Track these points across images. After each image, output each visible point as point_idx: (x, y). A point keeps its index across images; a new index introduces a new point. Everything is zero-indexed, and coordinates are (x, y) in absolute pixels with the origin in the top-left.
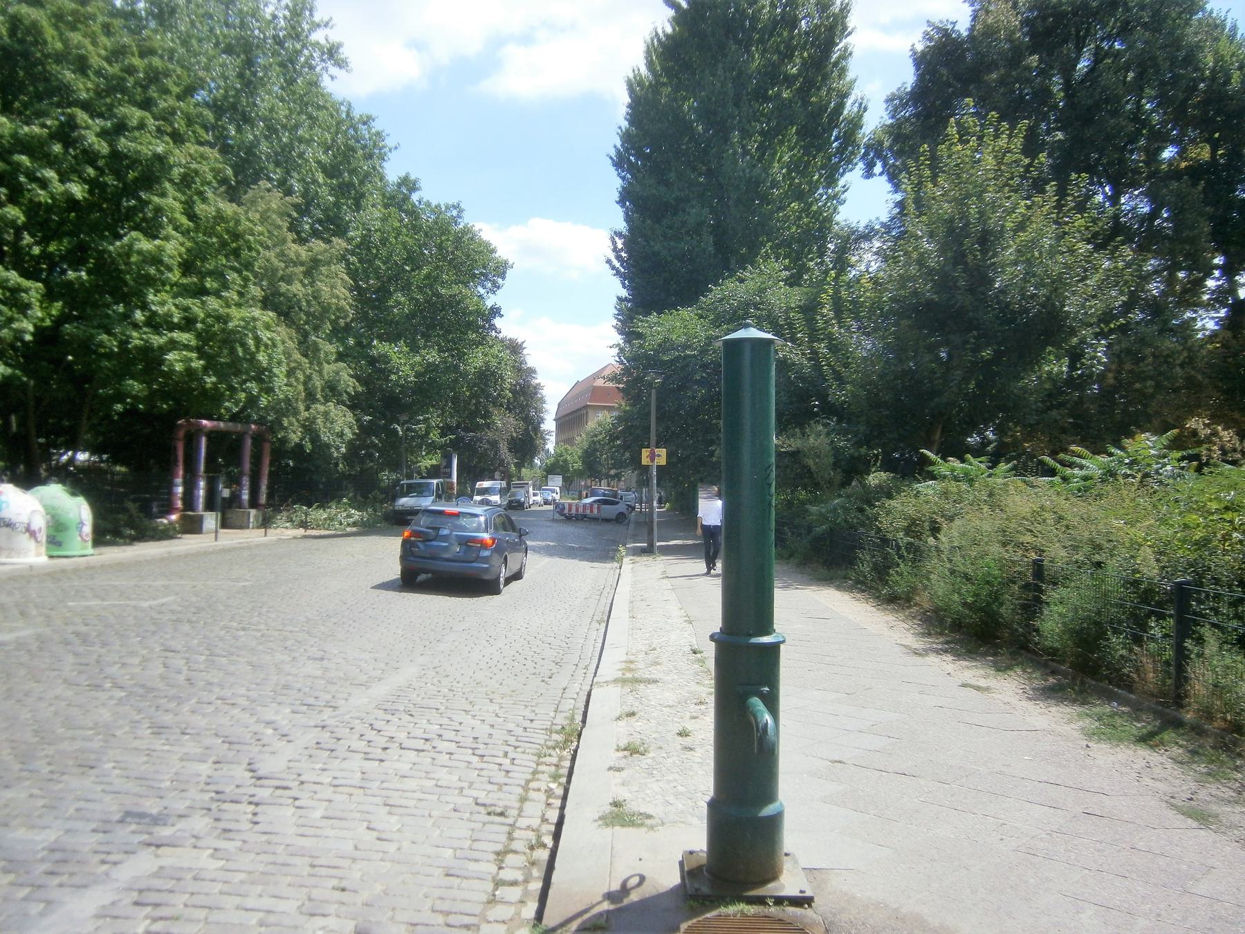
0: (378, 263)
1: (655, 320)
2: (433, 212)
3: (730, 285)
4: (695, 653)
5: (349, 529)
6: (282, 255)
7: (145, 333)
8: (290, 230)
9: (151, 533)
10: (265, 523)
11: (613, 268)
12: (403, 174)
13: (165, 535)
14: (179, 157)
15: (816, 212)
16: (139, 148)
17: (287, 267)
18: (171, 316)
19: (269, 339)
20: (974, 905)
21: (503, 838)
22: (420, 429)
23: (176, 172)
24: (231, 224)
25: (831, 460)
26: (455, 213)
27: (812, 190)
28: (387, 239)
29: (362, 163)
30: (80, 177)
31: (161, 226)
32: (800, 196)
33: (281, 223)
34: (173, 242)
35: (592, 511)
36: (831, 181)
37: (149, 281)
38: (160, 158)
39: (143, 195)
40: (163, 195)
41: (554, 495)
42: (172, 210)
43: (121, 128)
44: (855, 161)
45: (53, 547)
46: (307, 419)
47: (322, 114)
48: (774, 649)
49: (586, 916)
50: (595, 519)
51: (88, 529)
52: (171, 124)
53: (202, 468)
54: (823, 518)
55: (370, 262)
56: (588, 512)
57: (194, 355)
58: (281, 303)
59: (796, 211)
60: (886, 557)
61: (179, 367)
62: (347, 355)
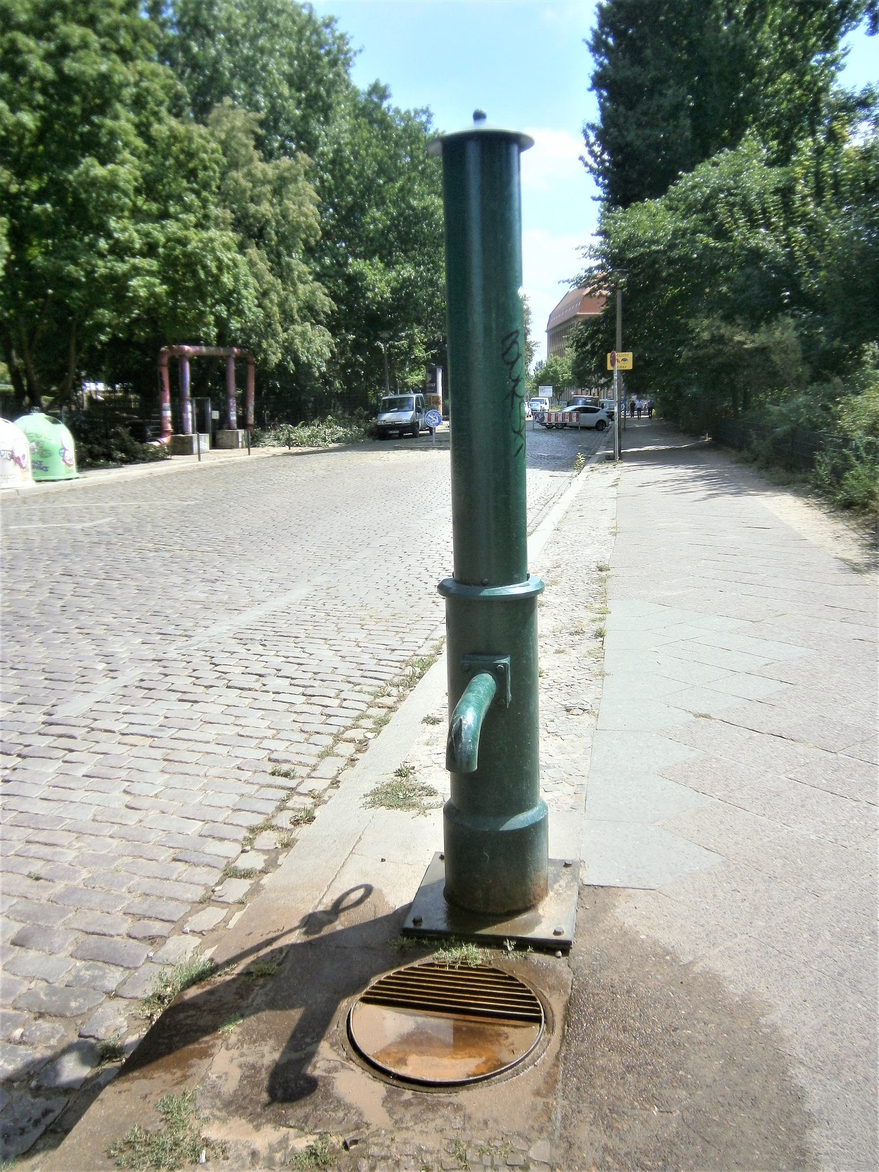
0: (350, 178)
1: (620, 215)
2: (402, 119)
3: (703, 168)
4: (601, 570)
5: (332, 446)
6: (249, 175)
7: (110, 261)
8: (256, 147)
9: (143, 456)
10: (253, 442)
11: (586, 165)
12: (372, 82)
13: (155, 457)
14: (123, 73)
15: (810, 83)
16: (83, 68)
17: (254, 187)
18: (132, 242)
19: (229, 259)
20: (806, 963)
21: (270, 808)
22: (403, 345)
23: (128, 93)
24: (186, 143)
25: (799, 355)
26: (424, 118)
27: (808, 53)
28: (358, 153)
29: (326, 71)
30: (30, 105)
31: (117, 151)
32: (790, 62)
33: (246, 141)
34: (127, 166)
35: (571, 420)
36: (830, 43)
37: (110, 208)
38: (105, 78)
39: (96, 119)
40: (116, 117)
41: (543, 405)
42: (126, 133)
43: (64, 50)
44: (860, 16)
45: (38, 471)
46: (286, 340)
47: (281, 20)
48: (527, 603)
49: (276, 945)
50: (575, 428)
51: (71, 454)
52: (117, 42)
53: (188, 393)
54: (784, 417)
55: (343, 178)
56: (567, 420)
57: (157, 281)
58: (251, 225)
59: (788, 83)
60: (845, 458)
61: (143, 293)
62: (325, 275)
